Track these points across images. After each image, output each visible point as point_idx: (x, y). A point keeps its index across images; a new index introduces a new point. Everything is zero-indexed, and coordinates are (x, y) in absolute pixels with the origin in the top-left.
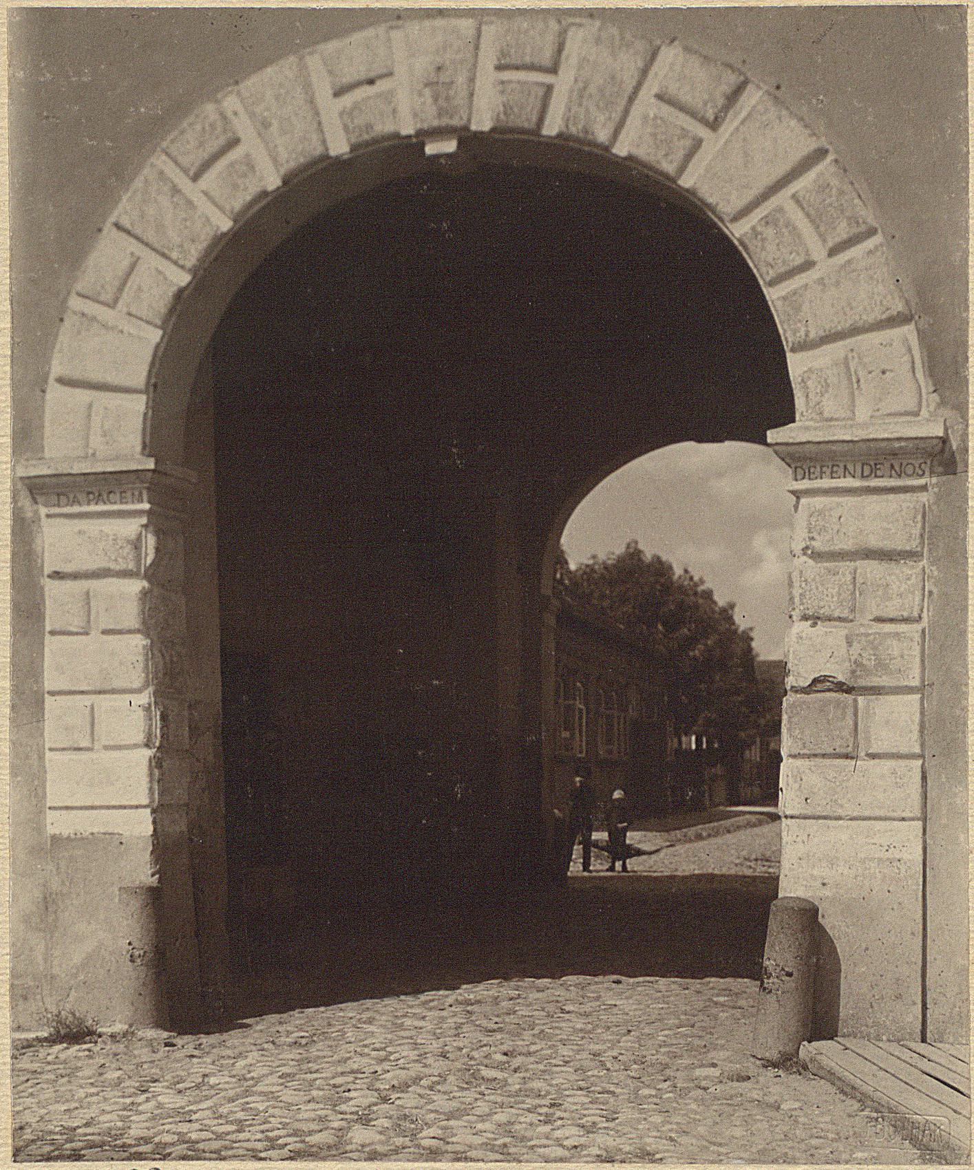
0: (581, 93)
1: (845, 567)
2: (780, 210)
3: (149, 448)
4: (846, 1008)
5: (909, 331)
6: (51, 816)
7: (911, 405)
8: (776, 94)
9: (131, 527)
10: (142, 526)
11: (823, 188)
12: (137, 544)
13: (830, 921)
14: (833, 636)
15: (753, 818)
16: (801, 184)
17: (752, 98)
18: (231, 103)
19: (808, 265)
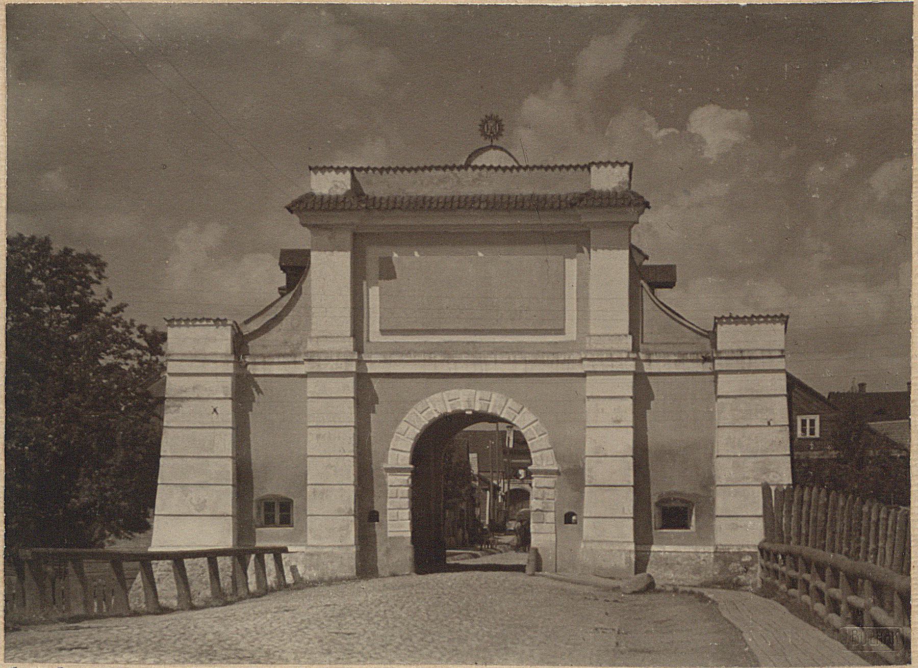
0: (495, 406)
1: (542, 490)
2: (530, 429)
3: (412, 463)
4: (543, 566)
5: (552, 451)
6: (389, 533)
7: (552, 463)
8: (529, 409)
9: (407, 478)
10: (105, 306)
11: (537, 425)
12: (408, 480)
13: (540, 551)
14: (540, 502)
15: (467, 556)
16: (534, 424)
17: (525, 409)
18: (427, 400)
19: (535, 438)
